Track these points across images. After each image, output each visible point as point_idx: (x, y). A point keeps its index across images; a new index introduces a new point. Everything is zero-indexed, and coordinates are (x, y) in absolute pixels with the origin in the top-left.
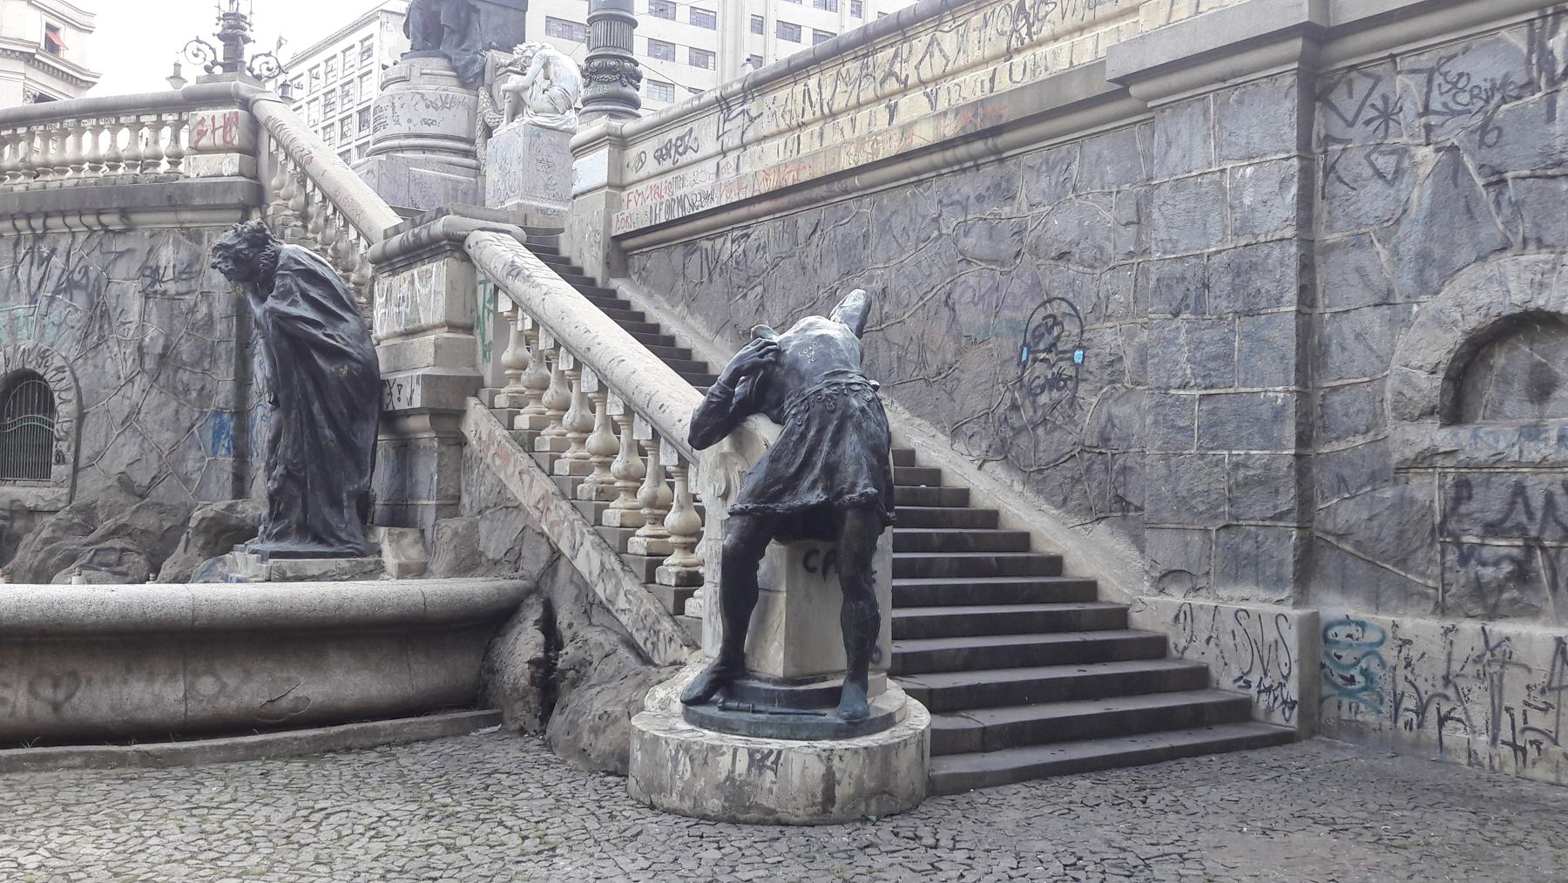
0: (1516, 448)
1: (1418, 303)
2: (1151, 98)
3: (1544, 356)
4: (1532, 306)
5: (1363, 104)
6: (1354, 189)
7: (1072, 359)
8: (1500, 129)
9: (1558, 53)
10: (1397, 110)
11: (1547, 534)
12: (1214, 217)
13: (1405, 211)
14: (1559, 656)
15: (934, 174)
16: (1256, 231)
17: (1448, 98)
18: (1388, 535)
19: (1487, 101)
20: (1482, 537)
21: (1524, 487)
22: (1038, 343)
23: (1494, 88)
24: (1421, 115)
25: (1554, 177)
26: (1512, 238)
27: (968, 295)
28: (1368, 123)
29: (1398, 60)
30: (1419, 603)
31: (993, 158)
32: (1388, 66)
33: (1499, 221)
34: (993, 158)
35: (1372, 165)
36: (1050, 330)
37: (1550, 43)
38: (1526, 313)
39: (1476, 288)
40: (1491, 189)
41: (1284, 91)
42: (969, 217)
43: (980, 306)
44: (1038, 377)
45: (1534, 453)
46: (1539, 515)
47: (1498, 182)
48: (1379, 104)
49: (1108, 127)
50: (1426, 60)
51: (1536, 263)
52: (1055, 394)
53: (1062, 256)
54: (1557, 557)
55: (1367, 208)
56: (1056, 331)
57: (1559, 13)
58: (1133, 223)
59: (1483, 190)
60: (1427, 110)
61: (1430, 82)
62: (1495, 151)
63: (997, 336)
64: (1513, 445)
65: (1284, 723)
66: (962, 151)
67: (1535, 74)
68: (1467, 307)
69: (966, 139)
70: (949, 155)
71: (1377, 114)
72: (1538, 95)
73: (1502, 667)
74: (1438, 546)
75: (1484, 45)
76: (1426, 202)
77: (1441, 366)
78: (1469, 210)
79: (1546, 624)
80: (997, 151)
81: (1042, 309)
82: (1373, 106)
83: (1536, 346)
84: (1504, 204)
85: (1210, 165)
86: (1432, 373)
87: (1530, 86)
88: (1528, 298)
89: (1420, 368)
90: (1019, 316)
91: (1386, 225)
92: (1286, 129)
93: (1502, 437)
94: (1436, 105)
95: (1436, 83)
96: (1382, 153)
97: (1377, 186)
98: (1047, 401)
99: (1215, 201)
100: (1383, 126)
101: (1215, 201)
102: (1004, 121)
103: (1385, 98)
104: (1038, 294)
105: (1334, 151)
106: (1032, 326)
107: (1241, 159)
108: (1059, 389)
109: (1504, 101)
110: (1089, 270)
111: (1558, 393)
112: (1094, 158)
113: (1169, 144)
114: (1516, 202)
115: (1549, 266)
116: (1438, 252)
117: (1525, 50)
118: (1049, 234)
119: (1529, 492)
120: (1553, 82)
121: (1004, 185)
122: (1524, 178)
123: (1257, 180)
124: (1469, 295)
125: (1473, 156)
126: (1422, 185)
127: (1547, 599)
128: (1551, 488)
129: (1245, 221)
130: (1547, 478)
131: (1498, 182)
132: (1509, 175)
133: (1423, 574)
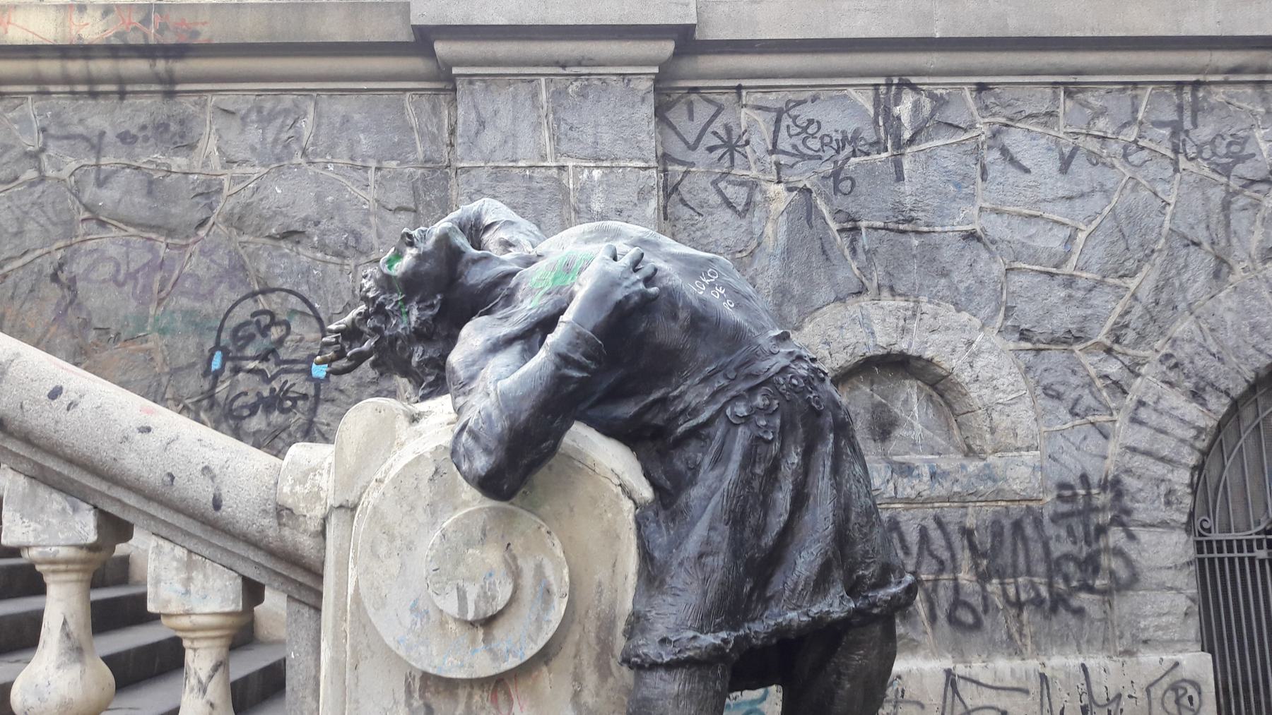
0: (891, 485)
2: (460, 64)
3: (885, 398)
4: (896, 349)
6: (699, 214)
7: (308, 372)
8: (851, 179)
9: (905, 119)
10: (742, 142)
11: (924, 568)
13: (759, 245)
14: (950, 688)
15: (34, 89)
19: (838, 152)
21: (898, 523)
22: (242, 348)
23: (845, 139)
25: (904, 232)
26: (867, 283)
27: (106, 270)
28: (711, 149)
29: (744, 93)
32: (732, 97)
33: (854, 266)
35: (720, 192)
36: (264, 331)
37: (897, 110)
38: (889, 354)
39: (842, 327)
41: (640, 94)
42: (103, 161)
43: (128, 288)
44: (245, 394)
45: (909, 490)
46: (915, 549)
47: (852, 229)
48: (722, 132)
49: (364, 86)
50: (772, 99)
51: (898, 309)
52: (276, 417)
53: (288, 235)
54: (935, 590)
55: (717, 235)
56: (275, 333)
57: (903, 84)
58: (406, 209)
59: (836, 234)
60: (774, 150)
61: (778, 121)
62: (850, 199)
63: (163, 332)
64: (888, 481)
66: (102, 66)
67: (882, 134)
68: (834, 345)
69: (113, 51)
70: (75, 67)
71: (719, 142)
72: (884, 155)
73: (895, 707)
75: (831, 98)
76: (782, 238)
78: (824, 252)
79: (926, 657)
80: (171, 79)
81: (249, 302)
82: (715, 133)
83: (875, 387)
84: (860, 251)
85: (544, 158)
87: (878, 145)
88: (893, 341)
90: (208, 308)
91: (739, 255)
92: (643, 136)
94: (785, 143)
95: (784, 124)
96: (730, 182)
97: (728, 215)
98: (263, 426)
99: (552, 201)
100: (727, 156)
102: (202, 39)
103: (728, 129)
104: (242, 281)
105: (675, 172)
106: (232, 323)
107: (585, 159)
108: (283, 411)
109: (854, 154)
110: (334, 259)
111: (899, 432)
112: (338, 120)
113: (482, 124)
114: (869, 251)
115: (910, 313)
116: (797, 289)
117: (872, 112)
119: (904, 528)
120: (898, 145)
121: (174, 127)
122: (876, 229)
123: (609, 185)
124: (836, 334)
125: (828, 201)
126: (776, 221)
127: (926, 633)
128: (923, 523)
130: (919, 513)
131: (852, 229)
132: (863, 224)
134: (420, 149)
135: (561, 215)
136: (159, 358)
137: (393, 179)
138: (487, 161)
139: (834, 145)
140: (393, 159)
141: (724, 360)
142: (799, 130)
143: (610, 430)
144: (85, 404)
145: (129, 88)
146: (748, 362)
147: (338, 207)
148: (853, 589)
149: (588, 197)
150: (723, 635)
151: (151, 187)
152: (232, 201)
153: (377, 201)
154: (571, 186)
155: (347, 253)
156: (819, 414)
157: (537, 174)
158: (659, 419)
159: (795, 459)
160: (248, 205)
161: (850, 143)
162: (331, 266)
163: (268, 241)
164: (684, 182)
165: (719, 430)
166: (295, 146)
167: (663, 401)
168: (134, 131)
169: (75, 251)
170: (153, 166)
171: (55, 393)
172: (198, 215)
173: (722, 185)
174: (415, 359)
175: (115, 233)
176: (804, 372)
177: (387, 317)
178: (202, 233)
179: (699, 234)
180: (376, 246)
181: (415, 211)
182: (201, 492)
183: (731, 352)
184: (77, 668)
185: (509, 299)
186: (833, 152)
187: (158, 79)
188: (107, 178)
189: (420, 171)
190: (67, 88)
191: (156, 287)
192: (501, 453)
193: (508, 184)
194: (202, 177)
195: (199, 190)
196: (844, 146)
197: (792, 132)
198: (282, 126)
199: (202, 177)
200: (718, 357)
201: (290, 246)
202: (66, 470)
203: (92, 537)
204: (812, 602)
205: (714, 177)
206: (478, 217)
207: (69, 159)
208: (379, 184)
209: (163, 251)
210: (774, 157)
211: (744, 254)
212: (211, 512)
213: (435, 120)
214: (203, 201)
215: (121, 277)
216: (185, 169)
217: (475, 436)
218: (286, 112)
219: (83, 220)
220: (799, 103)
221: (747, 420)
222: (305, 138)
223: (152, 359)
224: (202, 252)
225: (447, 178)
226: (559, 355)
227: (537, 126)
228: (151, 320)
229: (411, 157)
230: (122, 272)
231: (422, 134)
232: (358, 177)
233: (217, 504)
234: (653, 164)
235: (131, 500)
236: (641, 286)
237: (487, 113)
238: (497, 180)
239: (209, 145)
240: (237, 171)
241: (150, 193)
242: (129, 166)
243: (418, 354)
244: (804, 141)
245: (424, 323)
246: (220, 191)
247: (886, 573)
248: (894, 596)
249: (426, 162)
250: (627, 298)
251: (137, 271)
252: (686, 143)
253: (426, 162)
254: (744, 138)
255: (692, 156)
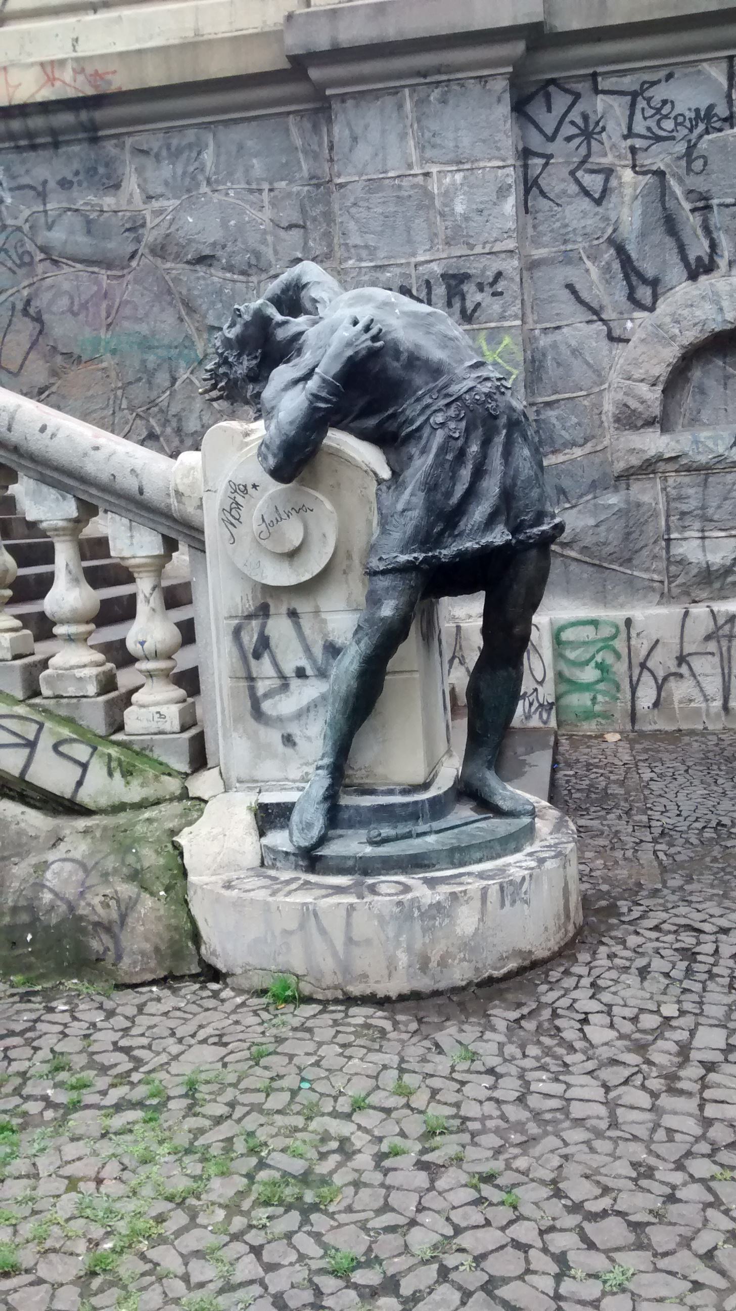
1: (632, 320)
5: (560, 123)
6: (558, 205)
8: (704, 157)
10: (598, 129)
12: (419, 223)
16: (471, 241)
17: (652, 123)
18: (614, 538)
19: (691, 131)
20: (703, 531)
24: (625, 137)
27: (64, 302)
28: (569, 139)
29: (599, 79)
30: (645, 597)
31: (80, 136)
34: (80, 136)
35: (578, 182)
40: (696, 214)
42: (49, 206)
43: (82, 317)
48: (579, 121)
50: (629, 83)
53: (203, 260)
55: (574, 224)
58: (296, 226)
59: (690, 214)
60: (630, 134)
63: (114, 352)
65: (542, 725)
66: (37, 122)
69: (45, 107)
71: (577, 131)
74: (664, 543)
76: (637, 223)
77: (662, 379)
82: (573, 123)
85: (410, 166)
86: (654, 385)
89: (642, 381)
91: (596, 242)
93: (720, 442)
94: (640, 127)
100: (585, 145)
101: (420, 207)
102: (113, 88)
103: (585, 117)
109: (707, 132)
110: (241, 278)
112: (234, 148)
118: (181, 233)
122: (727, 206)
123: (470, 187)
125: (681, 181)
129: (457, 228)
132: (715, 202)
133: (647, 570)
134: (305, 167)
135: (427, 220)
136: (113, 374)
137: (283, 198)
138: (362, 175)
139: (688, 124)
140: (282, 180)
141: (431, 385)
142: (653, 111)
143: (363, 435)
144: (60, 435)
145: (61, 138)
146: (446, 386)
147: (240, 228)
148: (515, 530)
149: (452, 200)
150: (416, 555)
151: (89, 226)
152: (155, 233)
153: (271, 220)
154: (436, 191)
155: (250, 272)
156: (496, 417)
157: (405, 183)
158: (392, 426)
159: (474, 448)
160: (168, 235)
161: (702, 121)
162: (238, 284)
163: (187, 267)
164: (543, 175)
165: (426, 431)
166: (200, 177)
167: (394, 416)
168: (70, 177)
169: (38, 289)
170: (89, 208)
171: (43, 429)
172: (131, 248)
173: (579, 174)
174: (249, 394)
175: (66, 269)
176: (486, 390)
177: (231, 366)
178: (134, 263)
179: (558, 224)
180: (274, 262)
181: (304, 227)
182: (129, 484)
183: (435, 380)
184: (77, 590)
185: (299, 352)
186: (686, 131)
187: (83, 127)
188: (53, 222)
189: (306, 188)
190: (12, 144)
191: (103, 314)
192: (281, 455)
193: (380, 195)
194: (128, 214)
195: (128, 226)
196: (697, 125)
197: (647, 115)
198: (188, 160)
199: (128, 214)
200: (427, 384)
201: (204, 269)
202: (56, 475)
203: (75, 514)
204: (482, 537)
205: (572, 167)
206: (299, 278)
207: (22, 207)
208: (273, 204)
209: (105, 282)
210: (629, 142)
211: (601, 240)
212: (138, 496)
213: (316, 139)
214: (131, 235)
215: (76, 308)
216: (114, 208)
217: (267, 447)
218: (190, 146)
219: (41, 261)
220: (653, 84)
221: (443, 425)
222: (208, 169)
223: (108, 376)
224: (136, 281)
225: (329, 193)
226: (313, 395)
227: (403, 136)
228: (103, 343)
229: (297, 175)
230: (76, 303)
231: (305, 152)
232: (255, 200)
233: (141, 492)
234: (510, 161)
235: (93, 491)
236: (369, 343)
237: (359, 131)
238: (370, 191)
239: (131, 184)
240: (156, 204)
241: (89, 232)
242: (69, 209)
243: (251, 389)
244: (658, 122)
245: (250, 369)
246: (143, 225)
247: (540, 517)
248: (543, 532)
249: (311, 179)
250: (357, 353)
251: (87, 302)
252: (545, 135)
253: (311, 179)
254: (601, 124)
255: (550, 148)
